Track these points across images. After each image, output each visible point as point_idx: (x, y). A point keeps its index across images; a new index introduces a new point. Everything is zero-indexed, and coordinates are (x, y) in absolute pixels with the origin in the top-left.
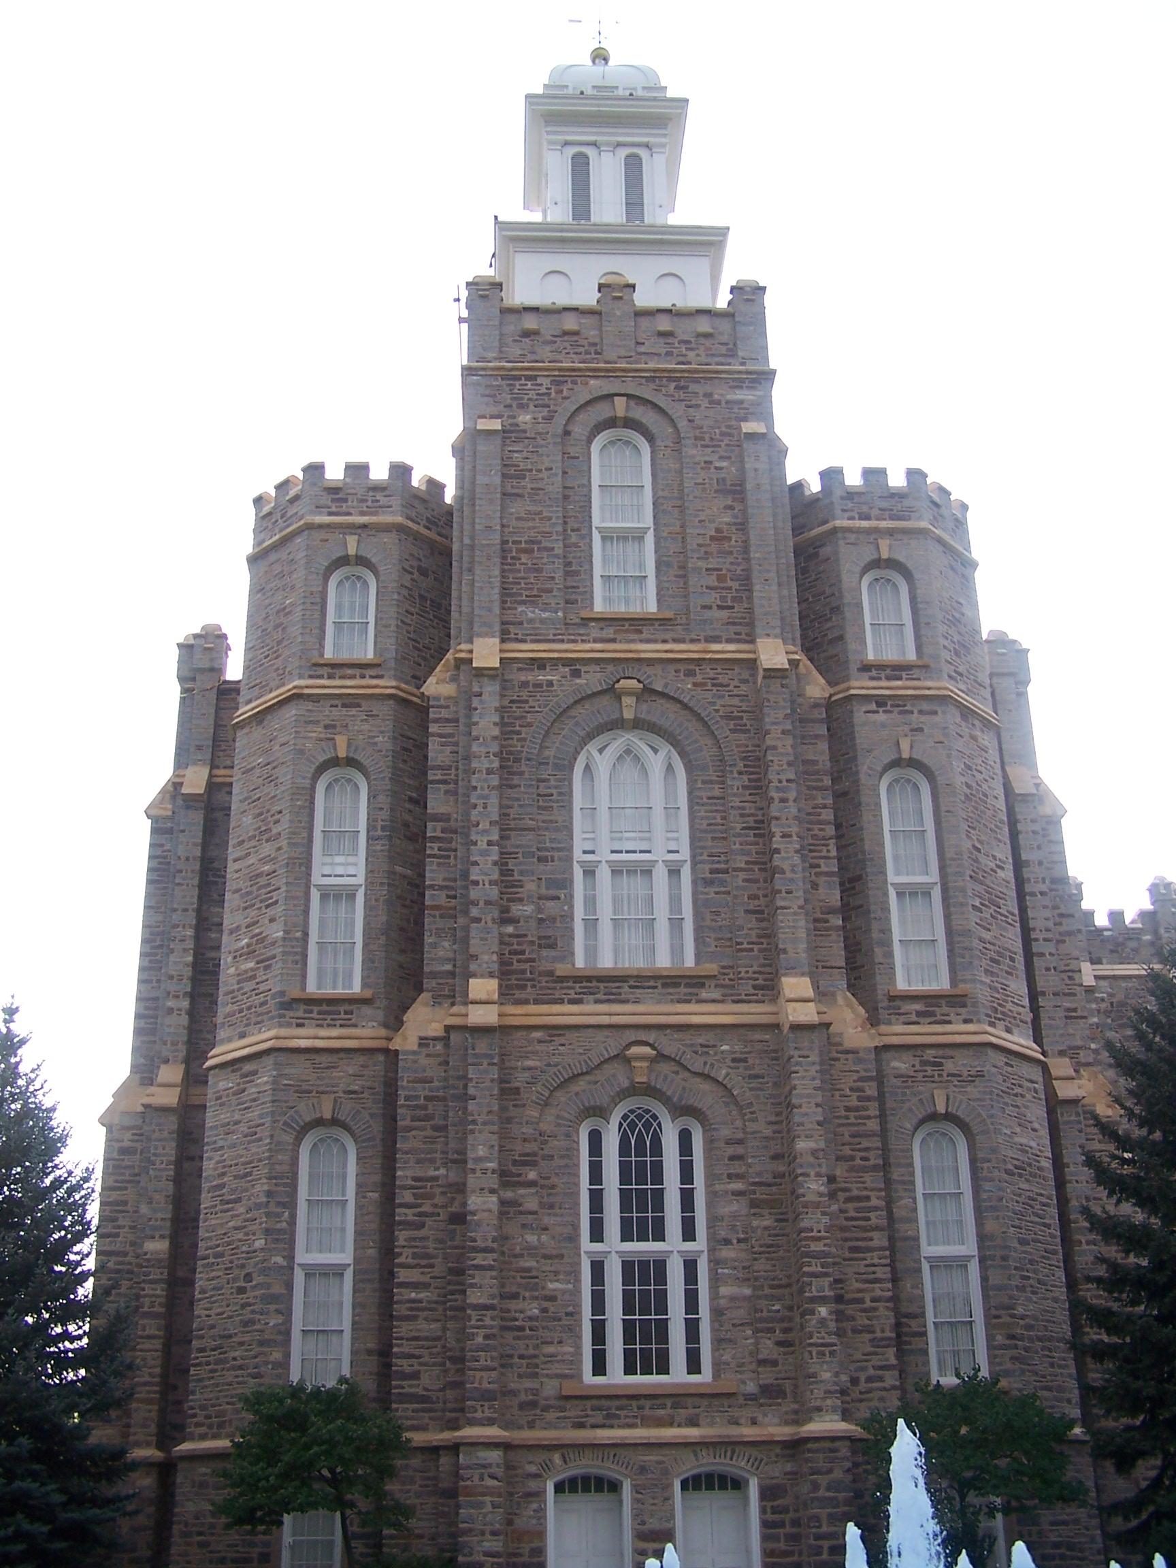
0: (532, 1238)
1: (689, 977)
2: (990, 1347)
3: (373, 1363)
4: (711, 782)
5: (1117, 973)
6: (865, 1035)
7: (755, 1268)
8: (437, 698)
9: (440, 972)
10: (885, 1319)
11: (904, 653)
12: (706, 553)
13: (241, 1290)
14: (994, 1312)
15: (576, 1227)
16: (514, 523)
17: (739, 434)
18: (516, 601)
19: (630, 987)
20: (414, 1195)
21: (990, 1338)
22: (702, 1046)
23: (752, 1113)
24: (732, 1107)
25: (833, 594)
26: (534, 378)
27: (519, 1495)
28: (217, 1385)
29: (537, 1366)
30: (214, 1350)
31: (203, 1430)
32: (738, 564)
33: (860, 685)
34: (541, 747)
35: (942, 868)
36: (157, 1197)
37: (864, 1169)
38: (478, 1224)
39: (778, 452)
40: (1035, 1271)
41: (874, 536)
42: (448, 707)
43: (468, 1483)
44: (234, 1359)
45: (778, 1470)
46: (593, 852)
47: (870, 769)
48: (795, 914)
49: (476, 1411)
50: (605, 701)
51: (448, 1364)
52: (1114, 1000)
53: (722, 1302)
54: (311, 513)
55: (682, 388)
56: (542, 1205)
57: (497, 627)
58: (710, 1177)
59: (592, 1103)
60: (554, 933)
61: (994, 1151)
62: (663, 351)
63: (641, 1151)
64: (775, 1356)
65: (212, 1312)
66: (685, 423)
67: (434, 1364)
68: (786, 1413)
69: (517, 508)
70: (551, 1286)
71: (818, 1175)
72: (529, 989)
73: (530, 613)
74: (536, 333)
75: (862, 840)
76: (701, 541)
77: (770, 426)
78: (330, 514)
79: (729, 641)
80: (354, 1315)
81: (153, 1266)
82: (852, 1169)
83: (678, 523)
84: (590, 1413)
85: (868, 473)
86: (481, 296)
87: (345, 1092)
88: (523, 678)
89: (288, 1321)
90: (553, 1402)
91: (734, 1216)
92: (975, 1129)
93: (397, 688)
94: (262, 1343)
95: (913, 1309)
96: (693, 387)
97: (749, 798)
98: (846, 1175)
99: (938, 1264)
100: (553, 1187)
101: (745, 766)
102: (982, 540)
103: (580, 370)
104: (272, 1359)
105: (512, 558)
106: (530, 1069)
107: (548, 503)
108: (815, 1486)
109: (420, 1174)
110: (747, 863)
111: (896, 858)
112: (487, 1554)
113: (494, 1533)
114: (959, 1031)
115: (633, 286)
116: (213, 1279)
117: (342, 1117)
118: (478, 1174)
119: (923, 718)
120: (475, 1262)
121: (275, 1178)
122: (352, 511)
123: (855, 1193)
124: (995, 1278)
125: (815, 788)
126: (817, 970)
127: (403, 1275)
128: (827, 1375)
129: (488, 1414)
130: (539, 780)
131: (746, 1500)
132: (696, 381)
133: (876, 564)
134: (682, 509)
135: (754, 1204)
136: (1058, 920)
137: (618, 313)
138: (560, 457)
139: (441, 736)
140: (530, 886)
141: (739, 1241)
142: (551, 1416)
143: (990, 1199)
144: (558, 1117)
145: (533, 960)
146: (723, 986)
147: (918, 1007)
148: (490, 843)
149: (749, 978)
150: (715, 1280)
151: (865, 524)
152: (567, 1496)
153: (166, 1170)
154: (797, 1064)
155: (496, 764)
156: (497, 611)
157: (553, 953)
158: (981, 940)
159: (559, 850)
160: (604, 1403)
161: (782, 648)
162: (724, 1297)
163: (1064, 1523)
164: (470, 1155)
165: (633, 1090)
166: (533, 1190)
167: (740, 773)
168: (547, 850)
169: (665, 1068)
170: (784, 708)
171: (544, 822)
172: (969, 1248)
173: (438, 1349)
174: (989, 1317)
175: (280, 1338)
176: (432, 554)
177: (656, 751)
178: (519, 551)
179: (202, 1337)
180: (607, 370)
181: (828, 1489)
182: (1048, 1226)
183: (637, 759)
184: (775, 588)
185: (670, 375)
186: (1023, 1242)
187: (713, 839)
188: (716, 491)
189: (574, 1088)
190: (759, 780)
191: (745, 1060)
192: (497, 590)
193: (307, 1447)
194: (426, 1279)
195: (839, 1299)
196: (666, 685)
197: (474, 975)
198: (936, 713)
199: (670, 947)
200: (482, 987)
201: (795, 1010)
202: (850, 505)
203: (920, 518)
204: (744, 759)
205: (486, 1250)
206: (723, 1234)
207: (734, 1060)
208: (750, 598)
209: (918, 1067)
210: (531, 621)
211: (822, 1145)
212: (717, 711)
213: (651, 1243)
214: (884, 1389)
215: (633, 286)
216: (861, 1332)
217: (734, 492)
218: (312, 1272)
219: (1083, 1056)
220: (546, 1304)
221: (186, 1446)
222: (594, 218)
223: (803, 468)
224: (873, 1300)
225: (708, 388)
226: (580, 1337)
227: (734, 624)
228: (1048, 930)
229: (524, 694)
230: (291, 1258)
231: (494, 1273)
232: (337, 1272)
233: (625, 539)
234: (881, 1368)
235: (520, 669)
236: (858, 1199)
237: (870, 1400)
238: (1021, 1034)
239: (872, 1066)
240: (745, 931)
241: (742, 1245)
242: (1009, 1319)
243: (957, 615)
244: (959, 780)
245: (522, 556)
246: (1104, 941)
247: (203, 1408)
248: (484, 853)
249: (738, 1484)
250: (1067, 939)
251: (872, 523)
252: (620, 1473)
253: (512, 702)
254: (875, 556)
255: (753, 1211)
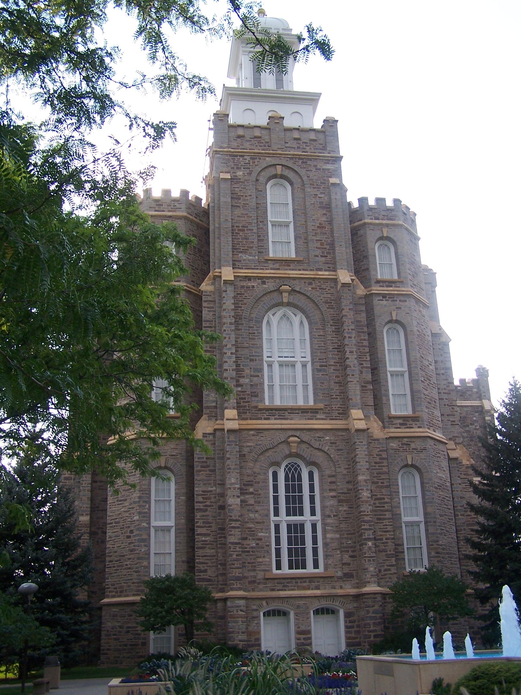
0: (252, 515)
1: (303, 409)
2: (429, 557)
3: (185, 566)
4: (319, 329)
5: (463, 404)
6: (382, 433)
7: (341, 526)
8: (205, 292)
9: (210, 406)
10: (391, 546)
11: (392, 275)
12: (316, 233)
13: (129, 537)
14: (431, 543)
15: (269, 510)
16: (236, 218)
17: (328, 183)
18: (238, 252)
19: (289, 413)
20: (203, 498)
21: (429, 553)
22: (318, 437)
23: (338, 464)
24: (330, 462)
25: (364, 251)
26: (243, 156)
27: (251, 618)
28: (119, 575)
29: (255, 567)
30: (117, 561)
31: (114, 593)
32: (329, 238)
33: (376, 289)
34: (250, 313)
35: (409, 365)
36: (84, 498)
37: (382, 487)
38: (233, 510)
39: (343, 190)
40: (445, 527)
41: (381, 227)
42: (210, 296)
43: (232, 613)
44: (127, 565)
45: (351, 606)
46: (271, 357)
47: (380, 324)
48: (355, 384)
49: (234, 585)
50: (276, 294)
51: (219, 566)
52: (462, 415)
53: (328, 540)
54: (147, 210)
55: (305, 162)
56: (255, 502)
57: (231, 263)
58: (322, 490)
59: (275, 460)
60: (256, 392)
61: (430, 479)
62: (296, 147)
63: (293, 480)
64: (349, 562)
65: (115, 546)
66: (306, 177)
67: (213, 566)
68: (354, 584)
69: (237, 212)
70: (260, 534)
71: (367, 490)
72: (248, 414)
73: (244, 257)
74: (243, 136)
75: (377, 353)
76: (313, 228)
77: (341, 180)
78: (156, 211)
79: (325, 270)
80: (176, 547)
81: (83, 527)
82: (377, 487)
83: (304, 220)
84: (276, 585)
85: (378, 200)
86: (220, 120)
87: (170, 455)
88: (242, 284)
89: (149, 550)
90: (262, 581)
91: (332, 506)
92: (423, 471)
93: (187, 286)
94: (139, 559)
95: (400, 542)
96: (309, 162)
97: (335, 336)
98: (375, 489)
99: (408, 524)
100: (259, 495)
101: (333, 323)
102: (422, 228)
103: (262, 153)
104: (143, 565)
105: (236, 233)
106: (250, 446)
107: (250, 210)
108: (368, 612)
109: (205, 489)
110: (335, 362)
111: (390, 361)
112: (240, 641)
113: (243, 633)
114: (416, 431)
115: (283, 118)
116: (115, 532)
117: (169, 465)
118: (232, 489)
119: (401, 303)
120: (232, 525)
121: (142, 491)
122: (165, 210)
123: (379, 496)
124: (431, 530)
125: (361, 332)
126: (364, 407)
127: (199, 531)
128: (372, 569)
129: (238, 586)
130: (249, 327)
131: (338, 619)
132: (310, 160)
133: (382, 238)
134: (305, 214)
135: (340, 501)
136: (447, 384)
137: (277, 129)
138: (255, 191)
139: (208, 308)
140: (247, 371)
141: (334, 516)
142: (261, 586)
143: (429, 499)
144: (261, 466)
145: (249, 402)
146: (325, 413)
147: (400, 421)
148: (232, 353)
149: (337, 410)
150: (324, 532)
151: (377, 221)
152: (320, 616)
153: (88, 487)
154: (358, 445)
155: (233, 321)
156: (231, 255)
157: (257, 399)
158: (424, 394)
159: (258, 356)
160: (282, 581)
161: (348, 274)
162: (328, 538)
163: (457, 624)
164: (228, 482)
165: (291, 455)
166: (252, 496)
167: (331, 325)
168: (253, 356)
169: (304, 446)
170: (349, 299)
171: (252, 344)
172: (420, 518)
173: (215, 560)
174: (428, 545)
175: (146, 556)
176: (198, 229)
177: (296, 315)
178: (239, 230)
179: (111, 556)
180: (274, 154)
181: (373, 613)
182: (449, 509)
183: (288, 318)
184: (344, 249)
185: (299, 157)
186: (441, 516)
187: (321, 352)
188: (319, 207)
189: (267, 454)
190: (339, 329)
191: (335, 443)
192: (231, 247)
193: (176, 600)
194: (209, 532)
195: (375, 539)
196: (300, 289)
197: (227, 408)
198: (406, 301)
199: (304, 397)
200: (230, 413)
201: (357, 423)
202: (371, 213)
203: (399, 220)
204: (332, 320)
205: (236, 520)
206: (327, 513)
207: (331, 443)
208: (334, 253)
209: (400, 446)
210: (244, 260)
211: (368, 478)
212: (322, 300)
213: (298, 517)
214: (391, 574)
215: (283, 118)
216: (381, 552)
217: (327, 208)
218: (157, 529)
219: (457, 441)
220: (257, 542)
221: (106, 600)
222: (263, 87)
223: (353, 198)
224: (386, 539)
225: (315, 163)
226: (271, 555)
227: (327, 263)
228: (445, 389)
229: (243, 291)
230: (149, 523)
231: (239, 530)
232: (167, 529)
233: (281, 226)
234: (390, 566)
235: (241, 280)
236: (380, 499)
237: (386, 578)
238: (439, 432)
239: (384, 446)
240: (334, 391)
241: (335, 518)
242: (437, 546)
243: (413, 260)
244: (415, 329)
245: (240, 232)
246: (458, 391)
247: (113, 585)
248: (229, 358)
249: (285, 614)
250: (451, 393)
251: (381, 221)
252: (290, 609)
253: (237, 294)
254: (381, 235)
255: (339, 504)
